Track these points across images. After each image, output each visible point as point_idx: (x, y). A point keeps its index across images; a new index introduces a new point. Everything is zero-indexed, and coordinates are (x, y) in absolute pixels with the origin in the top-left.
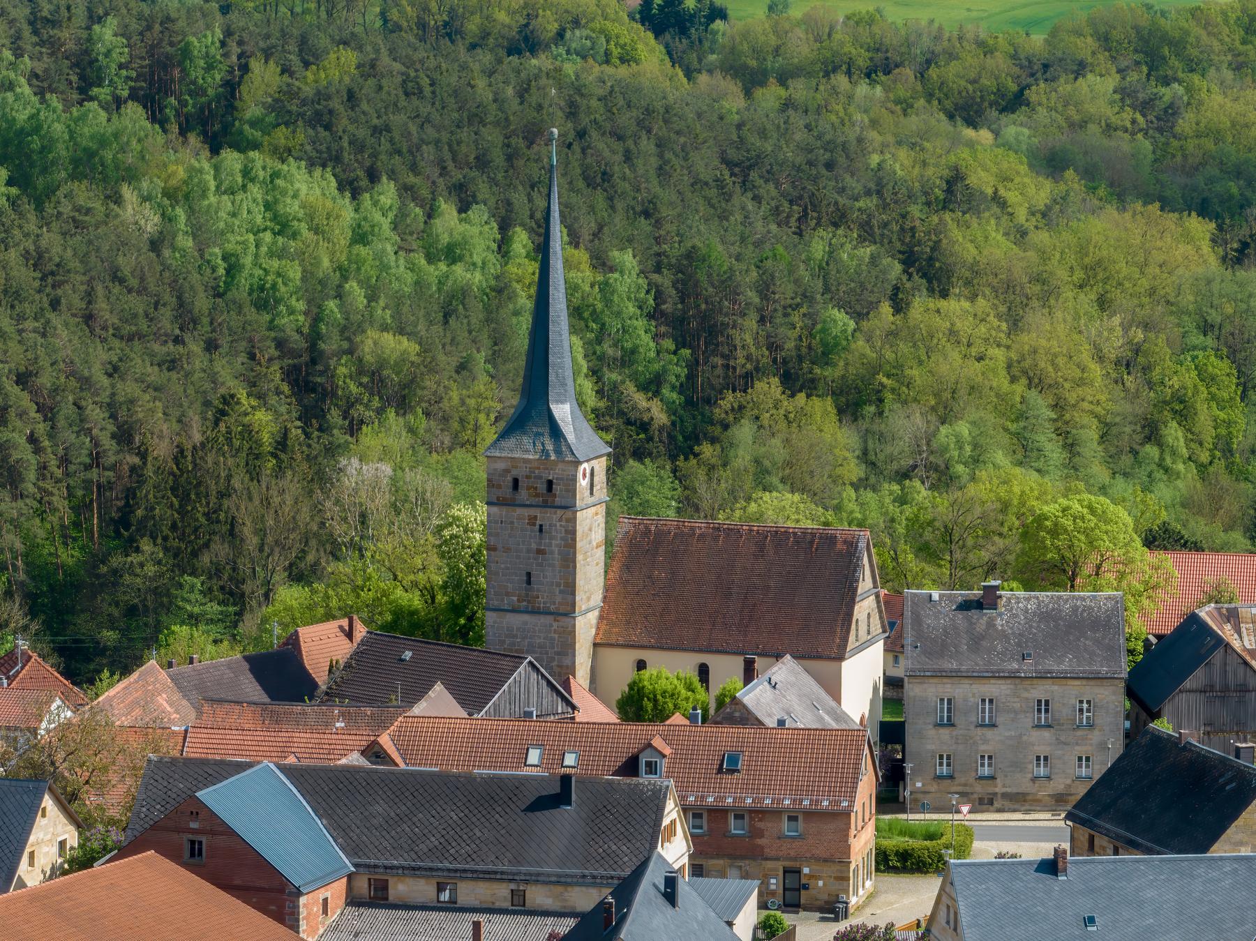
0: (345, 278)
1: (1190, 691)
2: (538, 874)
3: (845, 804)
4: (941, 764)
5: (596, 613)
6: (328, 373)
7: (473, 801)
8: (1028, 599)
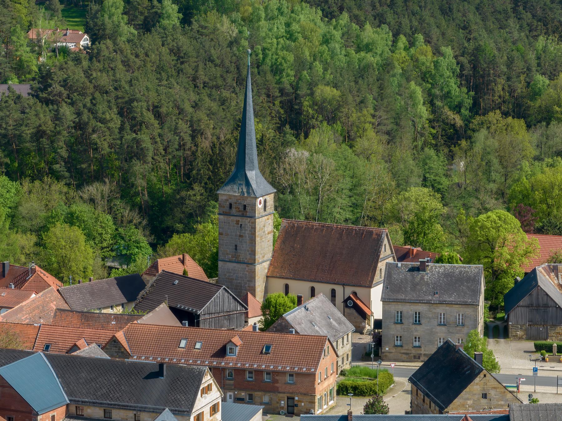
0: (315, 60)
1: (522, 306)
2: (145, 408)
3: (313, 370)
4: (397, 340)
5: (268, 263)
6: (301, 104)
7: (123, 373)
8: (440, 267)
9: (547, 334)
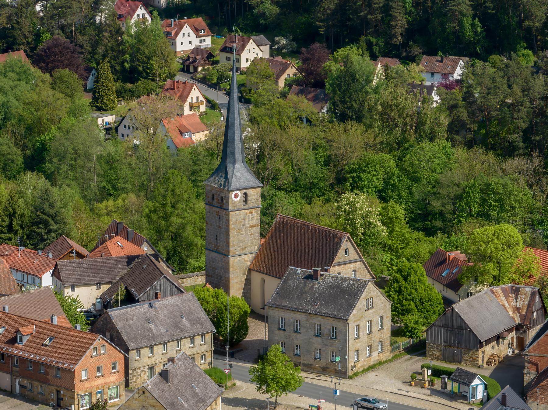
5: (253, 255)
9: (461, 357)
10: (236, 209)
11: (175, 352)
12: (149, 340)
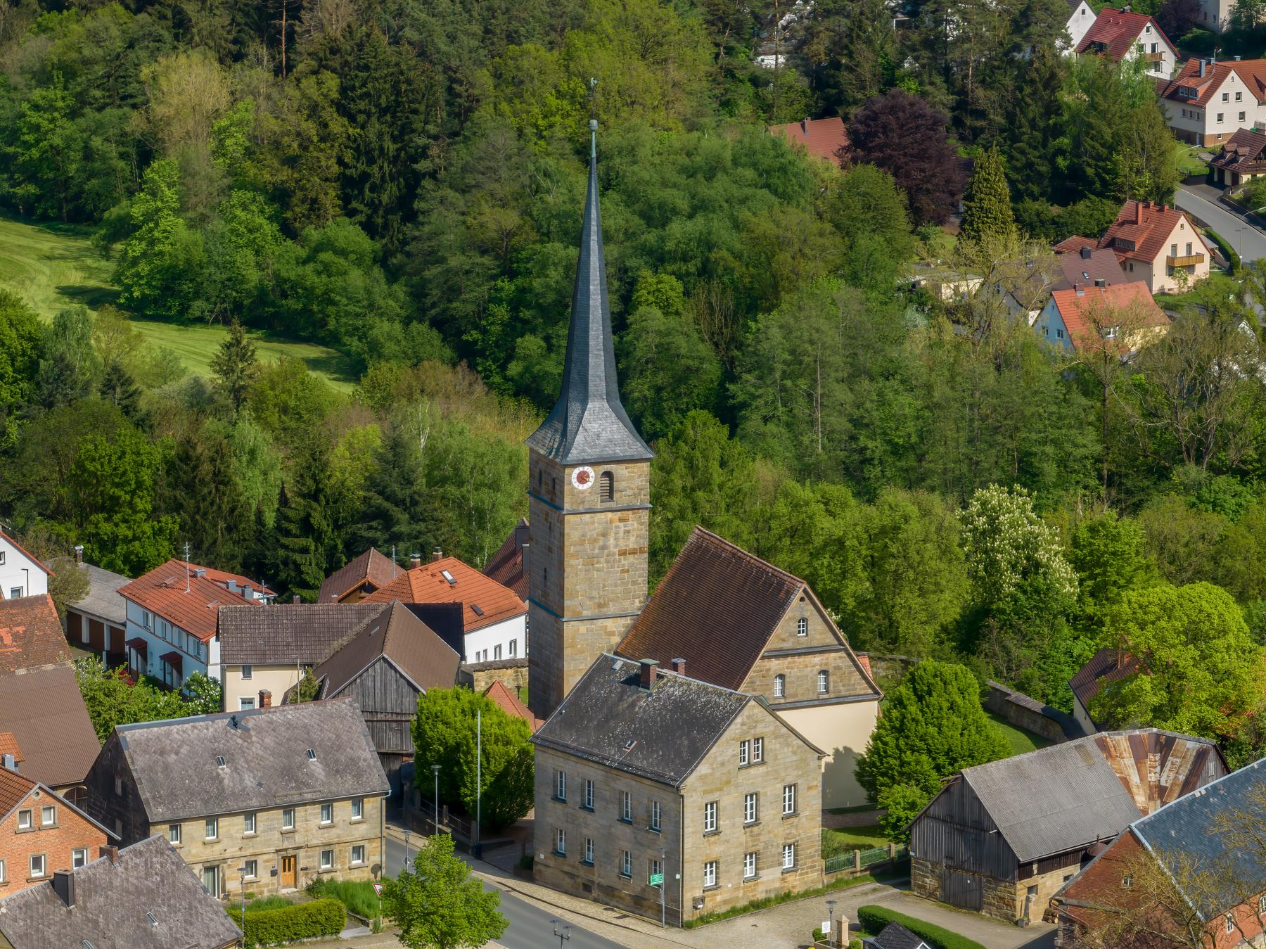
5: (628, 621)
10: (581, 509)
11: (278, 835)
12: (206, 802)
